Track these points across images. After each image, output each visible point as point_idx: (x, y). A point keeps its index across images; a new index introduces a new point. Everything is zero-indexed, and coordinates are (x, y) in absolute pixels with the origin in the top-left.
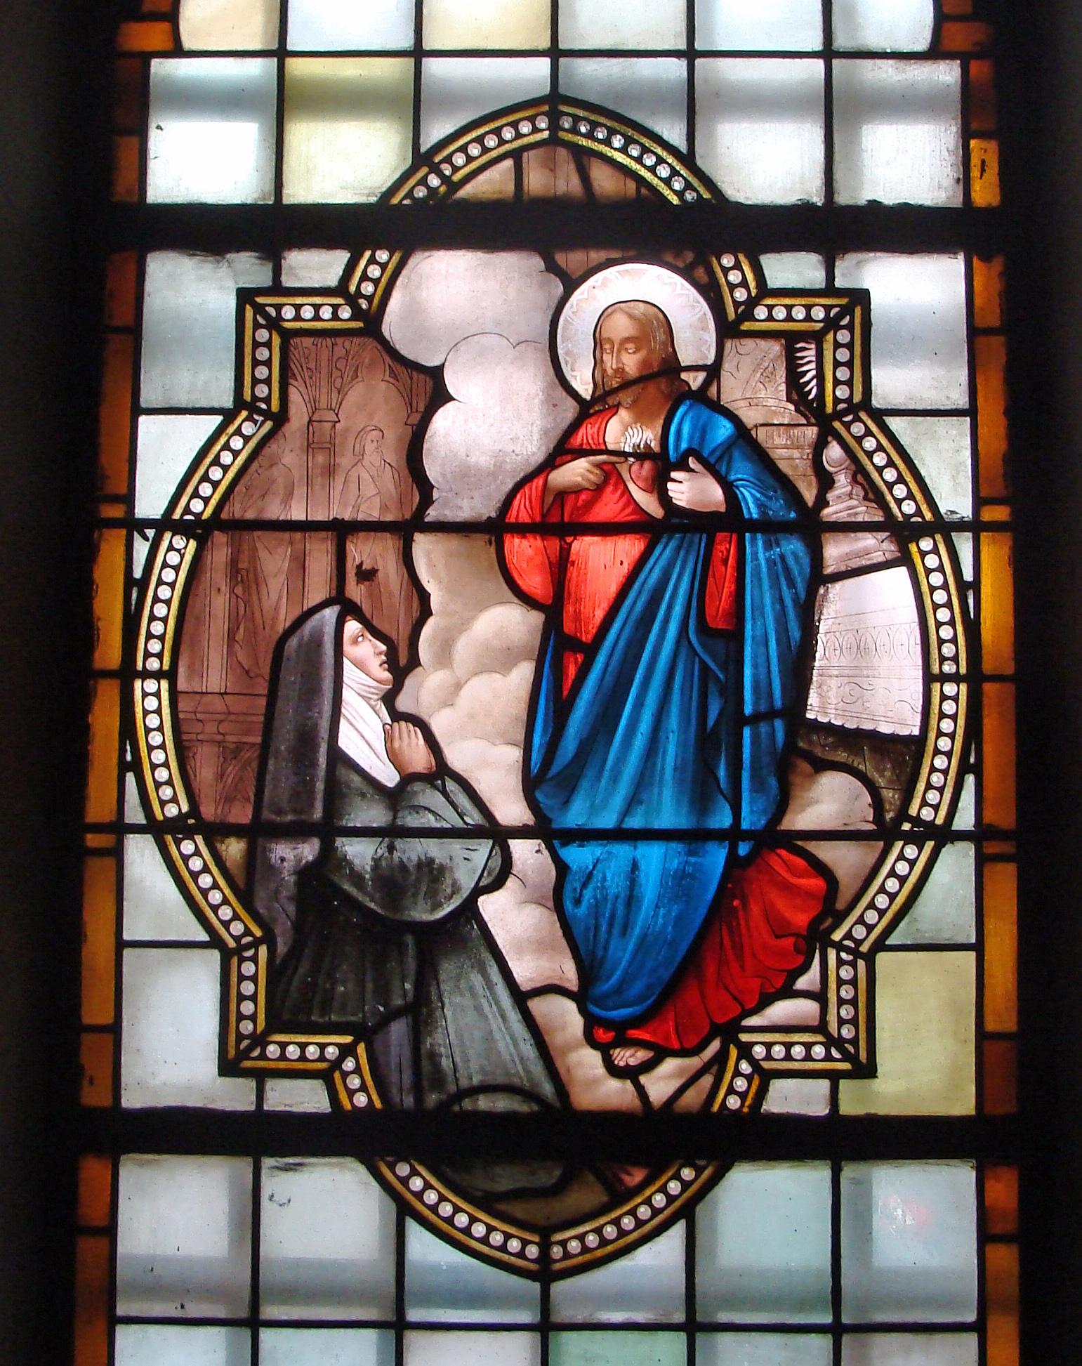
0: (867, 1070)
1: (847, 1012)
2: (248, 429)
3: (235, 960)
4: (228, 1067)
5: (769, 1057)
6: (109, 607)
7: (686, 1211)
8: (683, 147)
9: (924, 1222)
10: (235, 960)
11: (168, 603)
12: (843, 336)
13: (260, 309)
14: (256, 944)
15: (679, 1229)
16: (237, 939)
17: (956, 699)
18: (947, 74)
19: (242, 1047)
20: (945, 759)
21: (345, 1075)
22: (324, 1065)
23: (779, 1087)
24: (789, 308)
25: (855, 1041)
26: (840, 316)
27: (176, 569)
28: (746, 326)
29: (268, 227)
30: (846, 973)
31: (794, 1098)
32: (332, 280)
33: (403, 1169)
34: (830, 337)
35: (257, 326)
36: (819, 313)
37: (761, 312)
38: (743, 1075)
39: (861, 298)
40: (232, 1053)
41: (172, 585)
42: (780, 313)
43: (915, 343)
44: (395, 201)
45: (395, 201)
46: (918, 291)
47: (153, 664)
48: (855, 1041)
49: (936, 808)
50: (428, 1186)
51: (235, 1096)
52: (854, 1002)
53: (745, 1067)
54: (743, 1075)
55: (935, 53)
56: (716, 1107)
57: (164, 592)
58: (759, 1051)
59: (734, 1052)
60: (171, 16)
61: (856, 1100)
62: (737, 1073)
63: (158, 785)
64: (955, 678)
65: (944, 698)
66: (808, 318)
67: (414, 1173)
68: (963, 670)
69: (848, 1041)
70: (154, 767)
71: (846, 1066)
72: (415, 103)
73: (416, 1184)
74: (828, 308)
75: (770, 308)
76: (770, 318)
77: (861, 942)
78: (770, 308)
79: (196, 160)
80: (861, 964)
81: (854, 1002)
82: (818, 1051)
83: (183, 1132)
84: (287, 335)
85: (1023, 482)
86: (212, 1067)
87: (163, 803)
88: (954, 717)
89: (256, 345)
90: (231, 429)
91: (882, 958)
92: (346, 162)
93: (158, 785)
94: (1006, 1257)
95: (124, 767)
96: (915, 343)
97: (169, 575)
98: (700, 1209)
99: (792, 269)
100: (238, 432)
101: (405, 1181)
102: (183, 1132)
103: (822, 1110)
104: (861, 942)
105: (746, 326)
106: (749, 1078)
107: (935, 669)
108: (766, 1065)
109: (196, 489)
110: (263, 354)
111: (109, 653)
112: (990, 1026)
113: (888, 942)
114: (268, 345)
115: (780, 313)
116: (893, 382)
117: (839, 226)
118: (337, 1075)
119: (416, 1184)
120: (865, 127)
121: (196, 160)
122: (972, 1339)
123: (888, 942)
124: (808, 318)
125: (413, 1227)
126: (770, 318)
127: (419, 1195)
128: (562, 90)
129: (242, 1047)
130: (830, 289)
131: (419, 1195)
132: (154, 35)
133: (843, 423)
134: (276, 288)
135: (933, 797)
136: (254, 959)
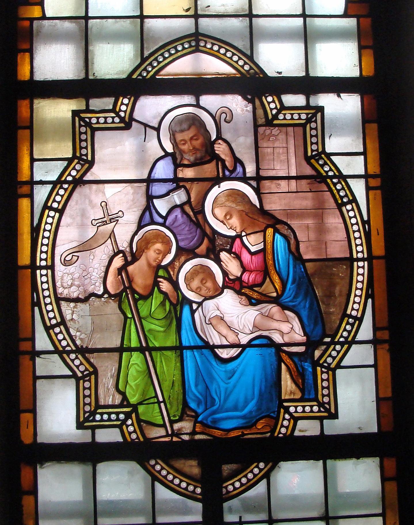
0: (334, 416)
1: (83, 137)
2: (329, 360)
3: (81, 381)
4: (80, 426)
5: (296, 412)
6: (380, 287)
7: (267, 476)
8: (249, 53)
9: (360, 477)
10: (81, 381)
11: (357, 289)
12: (87, 408)
13: (82, 119)
14: (313, 157)
15: (264, 481)
16: (82, 372)
17: (41, 260)
18: (351, 23)
19: (315, 118)
20: (360, 291)
21: (127, 426)
22: (283, 112)
23: (301, 424)
24: (292, 114)
25: (329, 403)
26: (312, 117)
27: (354, 302)
28: (275, 122)
29: (84, 87)
30: (84, 152)
31: (308, 428)
32: (300, 422)
33: (153, 462)
34: (308, 125)
35: (80, 126)
36: (304, 116)
37: (281, 117)
38: (287, 419)
39: (321, 109)
40: (82, 419)
41: (356, 296)
42: (288, 117)
43: (341, 128)
44: (134, 76)
45: (134, 76)
46: (342, 108)
47: (43, 263)
48: (329, 403)
49: (357, 310)
50: (162, 468)
51: (82, 437)
52: (81, 141)
53: (287, 416)
54: (287, 419)
55: (346, 15)
56: (132, 99)
57: (358, 292)
58: (292, 409)
59: (282, 411)
60: (41, 4)
61: (332, 427)
62: (284, 419)
63: (48, 312)
64: (41, 268)
65: (46, 260)
66: (300, 119)
67: (157, 463)
68: (366, 256)
69: (326, 403)
70: (46, 305)
71: (325, 414)
72: (142, 38)
73: (158, 467)
74: (307, 114)
75: (285, 115)
76: (285, 119)
77: (330, 364)
78: (285, 115)
79: (54, 61)
80: (78, 154)
81: (81, 141)
82: (94, 121)
83: (338, 86)
84: (316, 399)
85: (387, 180)
86: (74, 425)
87: (353, 209)
88: (363, 275)
89: (328, 395)
90: (337, 359)
91: (338, 372)
92: (114, 60)
93: (48, 312)
94: (392, 486)
95: (368, 222)
96: (341, 128)
97: (357, 299)
98: (139, 61)
99: (108, 436)
100: (74, 168)
101: (153, 467)
102: (338, 86)
103: (317, 432)
104: (330, 364)
105: (275, 122)
106: (289, 420)
107: (50, 271)
108: (296, 415)
109: (58, 191)
110: (83, 137)
111: (24, 259)
112: (28, 132)
113: (342, 365)
114: (323, 396)
115: (288, 117)
116: (332, 145)
117: (310, 85)
118: (124, 427)
119: (158, 467)
120: (317, 45)
121: (54, 61)
122: (381, 518)
123: (342, 365)
124: (300, 119)
125: (157, 485)
126: (285, 119)
127: (159, 472)
128: (200, 31)
129: (315, 118)
130: (93, 429)
131: (159, 472)
132: (36, 12)
133: (88, 370)
134: (88, 110)
135: (356, 306)
136: (89, 381)
